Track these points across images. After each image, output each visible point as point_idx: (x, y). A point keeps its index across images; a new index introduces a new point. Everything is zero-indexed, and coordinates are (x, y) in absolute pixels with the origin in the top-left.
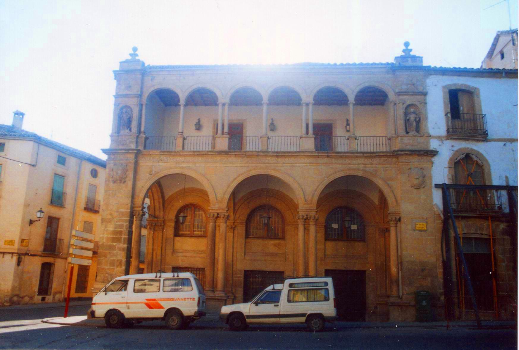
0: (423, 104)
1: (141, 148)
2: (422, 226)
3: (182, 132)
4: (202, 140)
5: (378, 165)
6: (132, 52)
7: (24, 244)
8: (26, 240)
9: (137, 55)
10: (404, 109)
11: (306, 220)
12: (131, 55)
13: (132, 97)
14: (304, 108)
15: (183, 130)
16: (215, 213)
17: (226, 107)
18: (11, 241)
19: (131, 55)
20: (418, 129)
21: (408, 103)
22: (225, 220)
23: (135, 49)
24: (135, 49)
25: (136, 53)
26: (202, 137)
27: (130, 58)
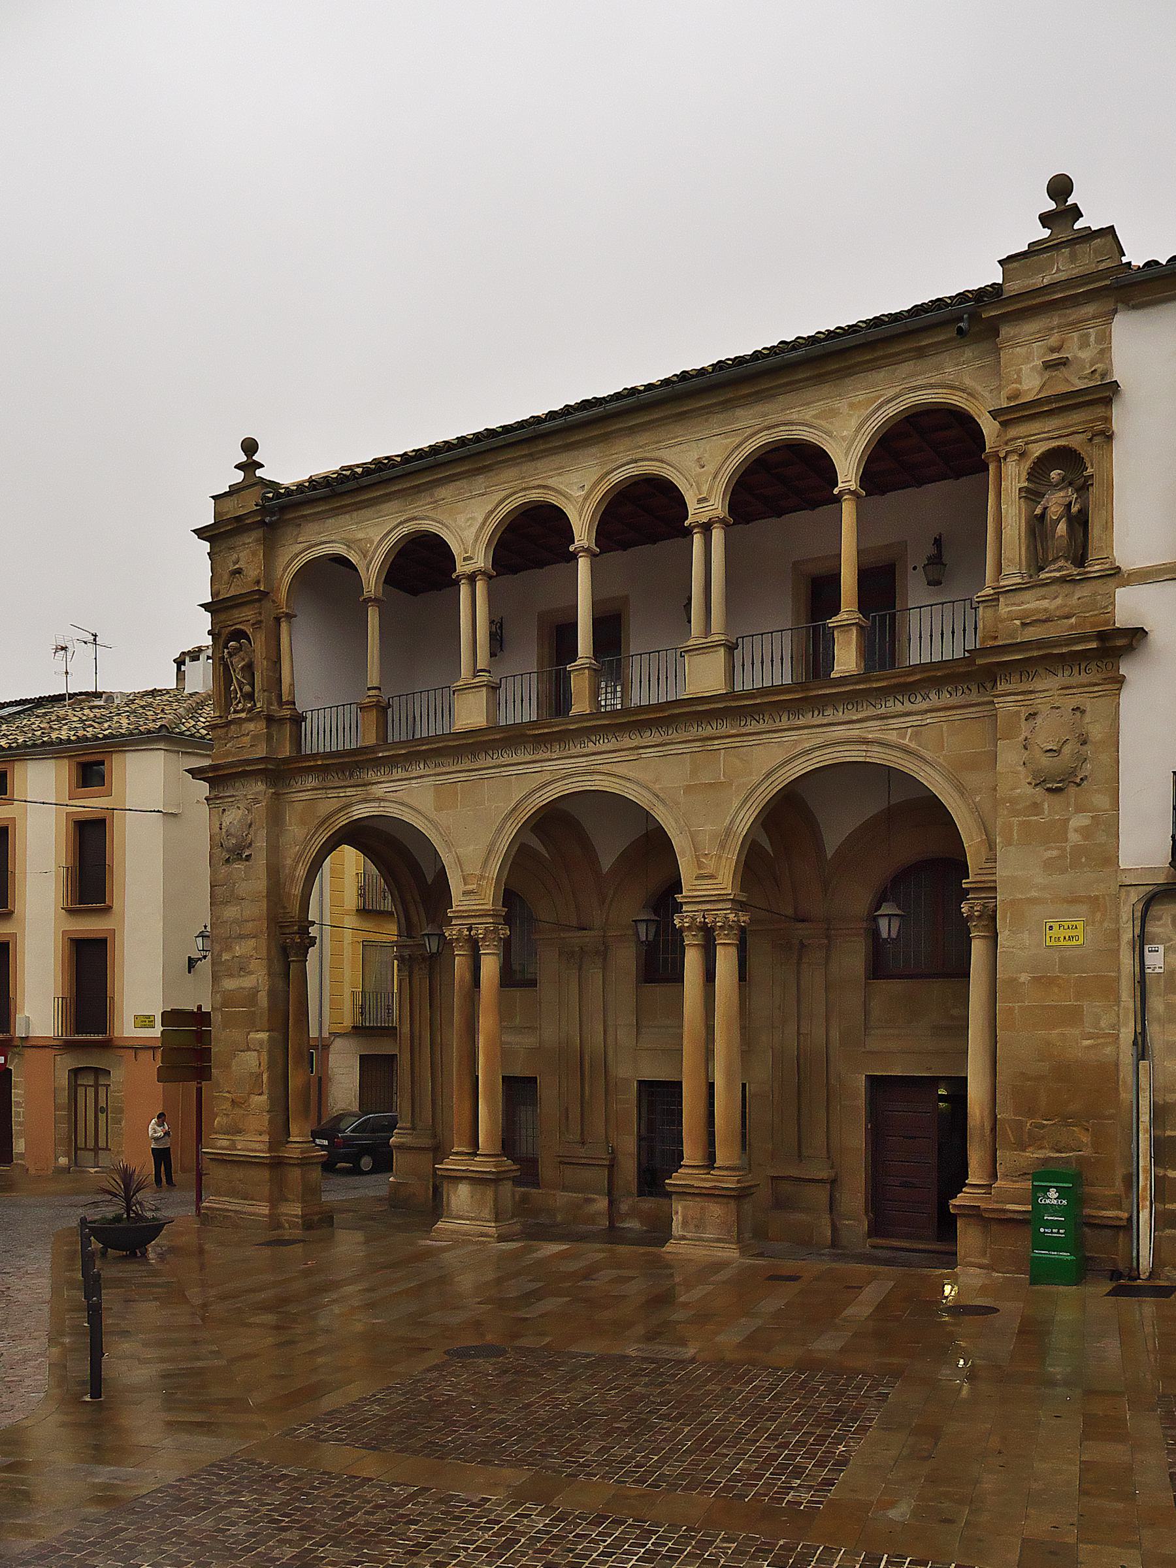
10: (1024, 475)
21: (1037, 450)
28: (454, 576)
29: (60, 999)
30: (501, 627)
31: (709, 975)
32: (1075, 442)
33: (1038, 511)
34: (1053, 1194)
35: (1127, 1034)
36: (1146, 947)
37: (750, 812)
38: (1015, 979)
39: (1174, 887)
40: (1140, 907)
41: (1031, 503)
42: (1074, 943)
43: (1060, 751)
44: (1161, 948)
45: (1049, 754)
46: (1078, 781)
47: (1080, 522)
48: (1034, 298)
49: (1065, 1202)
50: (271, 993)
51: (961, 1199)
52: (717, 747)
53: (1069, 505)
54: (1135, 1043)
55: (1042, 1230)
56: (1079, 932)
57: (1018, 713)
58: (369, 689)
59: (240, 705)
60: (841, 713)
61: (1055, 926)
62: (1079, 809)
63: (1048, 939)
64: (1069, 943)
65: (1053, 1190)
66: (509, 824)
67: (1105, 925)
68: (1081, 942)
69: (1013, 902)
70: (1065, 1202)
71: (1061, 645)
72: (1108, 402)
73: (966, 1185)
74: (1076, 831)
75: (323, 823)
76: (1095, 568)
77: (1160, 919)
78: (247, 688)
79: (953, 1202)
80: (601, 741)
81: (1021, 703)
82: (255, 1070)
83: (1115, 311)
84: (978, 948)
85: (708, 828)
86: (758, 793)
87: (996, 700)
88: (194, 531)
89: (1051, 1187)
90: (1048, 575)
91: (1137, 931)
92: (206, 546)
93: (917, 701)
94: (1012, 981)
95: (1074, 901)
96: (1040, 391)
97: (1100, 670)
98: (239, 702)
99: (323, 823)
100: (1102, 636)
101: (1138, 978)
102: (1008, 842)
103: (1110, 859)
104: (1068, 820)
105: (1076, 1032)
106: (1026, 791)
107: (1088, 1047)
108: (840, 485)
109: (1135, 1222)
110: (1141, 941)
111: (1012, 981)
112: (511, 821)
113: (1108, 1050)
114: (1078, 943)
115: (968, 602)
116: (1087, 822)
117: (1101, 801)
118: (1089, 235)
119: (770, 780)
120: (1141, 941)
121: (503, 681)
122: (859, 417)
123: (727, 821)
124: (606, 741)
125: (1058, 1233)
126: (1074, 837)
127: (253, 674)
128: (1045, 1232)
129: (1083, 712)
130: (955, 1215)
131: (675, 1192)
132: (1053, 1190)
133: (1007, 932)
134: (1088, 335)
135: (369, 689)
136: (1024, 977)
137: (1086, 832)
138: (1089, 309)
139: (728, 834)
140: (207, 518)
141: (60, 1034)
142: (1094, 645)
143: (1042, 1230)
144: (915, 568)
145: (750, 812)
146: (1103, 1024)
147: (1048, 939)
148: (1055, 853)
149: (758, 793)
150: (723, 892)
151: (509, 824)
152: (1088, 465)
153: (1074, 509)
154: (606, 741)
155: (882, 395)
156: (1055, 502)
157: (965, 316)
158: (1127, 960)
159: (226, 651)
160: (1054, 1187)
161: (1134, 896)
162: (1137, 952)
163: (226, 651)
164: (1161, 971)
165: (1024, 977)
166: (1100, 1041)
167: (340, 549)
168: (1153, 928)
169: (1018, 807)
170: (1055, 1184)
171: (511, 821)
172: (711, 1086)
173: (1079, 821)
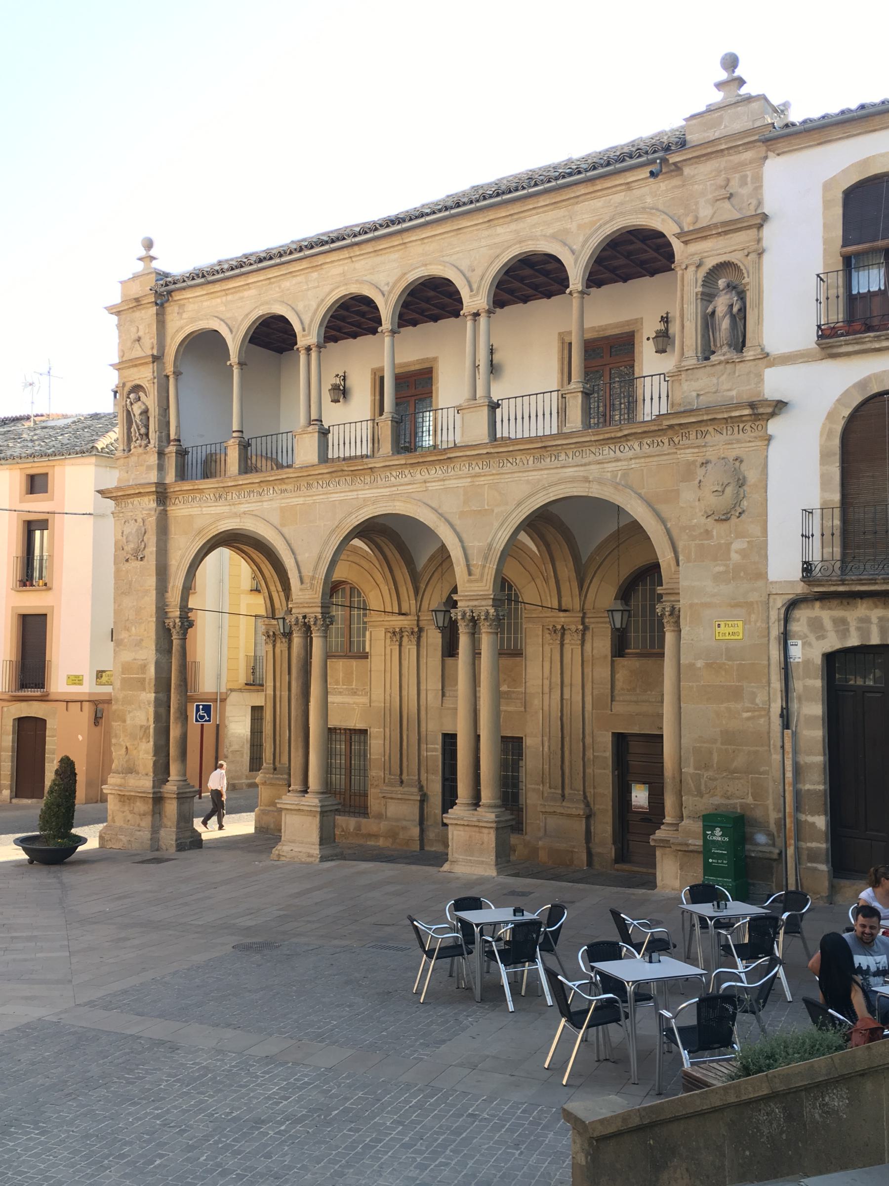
0: (753, 256)
1: (170, 477)
2: (731, 630)
3: (179, 441)
4: (259, 444)
5: (633, 461)
6: (723, 75)
7: (104, 679)
8: (107, 673)
9: (741, 82)
10: (700, 282)
11: (474, 622)
12: (719, 86)
13: (719, 234)
14: (469, 324)
15: (320, 416)
16: (467, 610)
17: (483, 320)
18: (76, 676)
19: (719, 86)
20: (739, 343)
21: (710, 263)
22: (318, 630)
23: (731, 62)
24: (731, 62)
25: (738, 72)
26: (519, 400)
27: (717, 97)
28: (228, 363)
29: (8, 662)
30: (344, 380)
31: (476, 654)
32: (734, 258)
33: (710, 310)
34: (718, 832)
35: (776, 707)
36: (789, 642)
37: (506, 533)
38: (694, 664)
39: (888, 576)
40: (783, 611)
41: (705, 302)
42: (736, 637)
43: (723, 492)
44: (800, 642)
45: (716, 494)
46: (737, 514)
47: (739, 318)
48: (706, 148)
49: (727, 839)
50: (157, 664)
51: (660, 834)
52: (482, 483)
53: (731, 306)
54: (782, 716)
55: (710, 860)
56: (740, 630)
57: (694, 462)
58: (234, 432)
59: (138, 442)
60: (571, 459)
61: (722, 625)
62: (740, 535)
63: (717, 634)
64: (732, 637)
65: (718, 829)
66: (333, 538)
67: (759, 624)
68: (741, 637)
69: (691, 606)
70: (727, 839)
71: (723, 412)
72: (760, 226)
73: (663, 824)
74: (736, 552)
75: (199, 533)
76: (749, 354)
77: (798, 620)
78: (143, 431)
79: (652, 837)
80: (400, 476)
81: (697, 455)
82: (144, 723)
83: (766, 158)
84: (669, 637)
85: (476, 544)
86: (511, 518)
87: (679, 452)
88: (105, 308)
89: (717, 827)
90: (716, 358)
91: (782, 630)
92: (115, 319)
93: (625, 451)
94: (692, 666)
95: (737, 605)
96: (711, 218)
97: (753, 430)
98: (137, 440)
99: (199, 533)
100: (752, 405)
101: (783, 666)
102: (688, 560)
103: (762, 575)
104: (732, 543)
105: (739, 706)
106: (699, 520)
107: (748, 719)
108: (571, 286)
109: (784, 856)
110: (785, 638)
111: (692, 666)
112: (335, 536)
113: (762, 721)
114: (739, 638)
115: (662, 376)
116: (745, 545)
117: (754, 529)
118: (749, 99)
119: (520, 509)
120: (785, 638)
121: (331, 428)
122: (584, 235)
123: (489, 540)
124: (404, 476)
125: (722, 863)
126: (735, 557)
127: (148, 418)
128: (712, 862)
129: (741, 461)
130: (655, 847)
131: (452, 824)
132: (718, 829)
133: (687, 628)
134: (746, 176)
135: (234, 432)
136: (700, 664)
137: (743, 553)
138: (748, 155)
139: (490, 549)
140: (116, 298)
141: (7, 690)
142: (747, 412)
143: (710, 860)
144: (648, 339)
145: (506, 533)
146: (757, 701)
147: (717, 634)
148: (722, 569)
149: (511, 518)
150: (486, 593)
151: (333, 538)
152: (746, 275)
153: (735, 309)
154: (404, 476)
155: (600, 219)
156: (721, 304)
157: (658, 161)
158: (775, 653)
159: (128, 400)
160: (719, 827)
161: (779, 603)
162: (782, 646)
163: (128, 400)
164: (800, 660)
165: (700, 664)
166: (756, 713)
167: (215, 325)
168: (794, 627)
169: (694, 533)
170: (720, 825)
171: (335, 536)
172: (478, 738)
173: (738, 545)
